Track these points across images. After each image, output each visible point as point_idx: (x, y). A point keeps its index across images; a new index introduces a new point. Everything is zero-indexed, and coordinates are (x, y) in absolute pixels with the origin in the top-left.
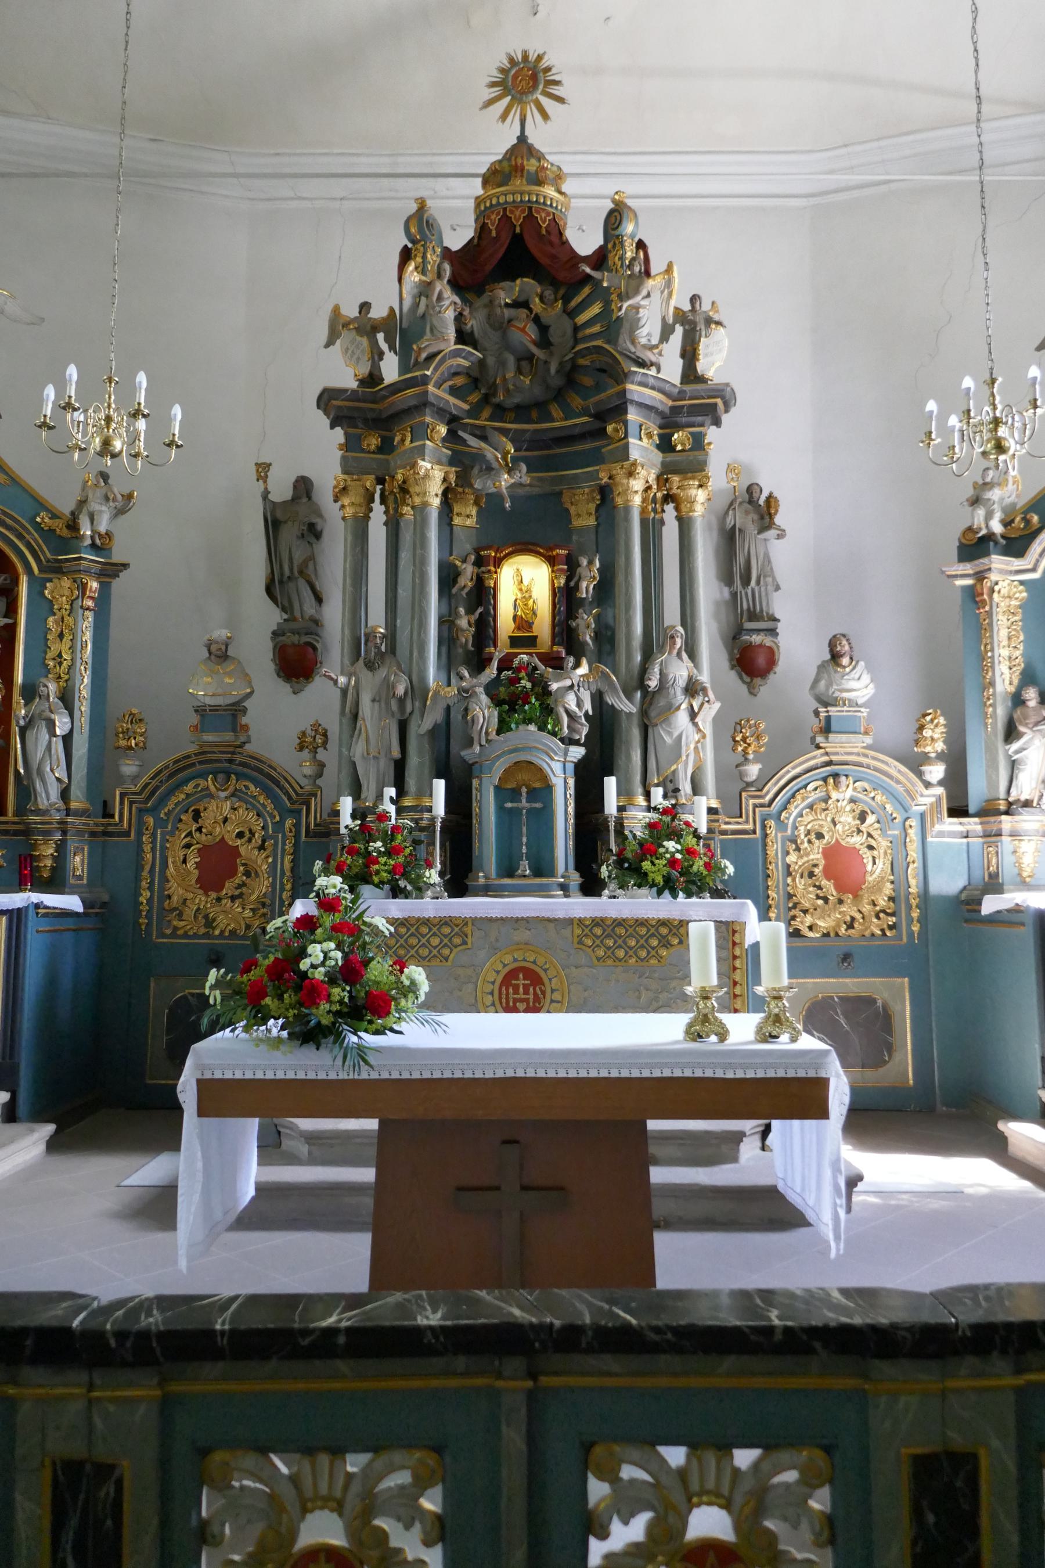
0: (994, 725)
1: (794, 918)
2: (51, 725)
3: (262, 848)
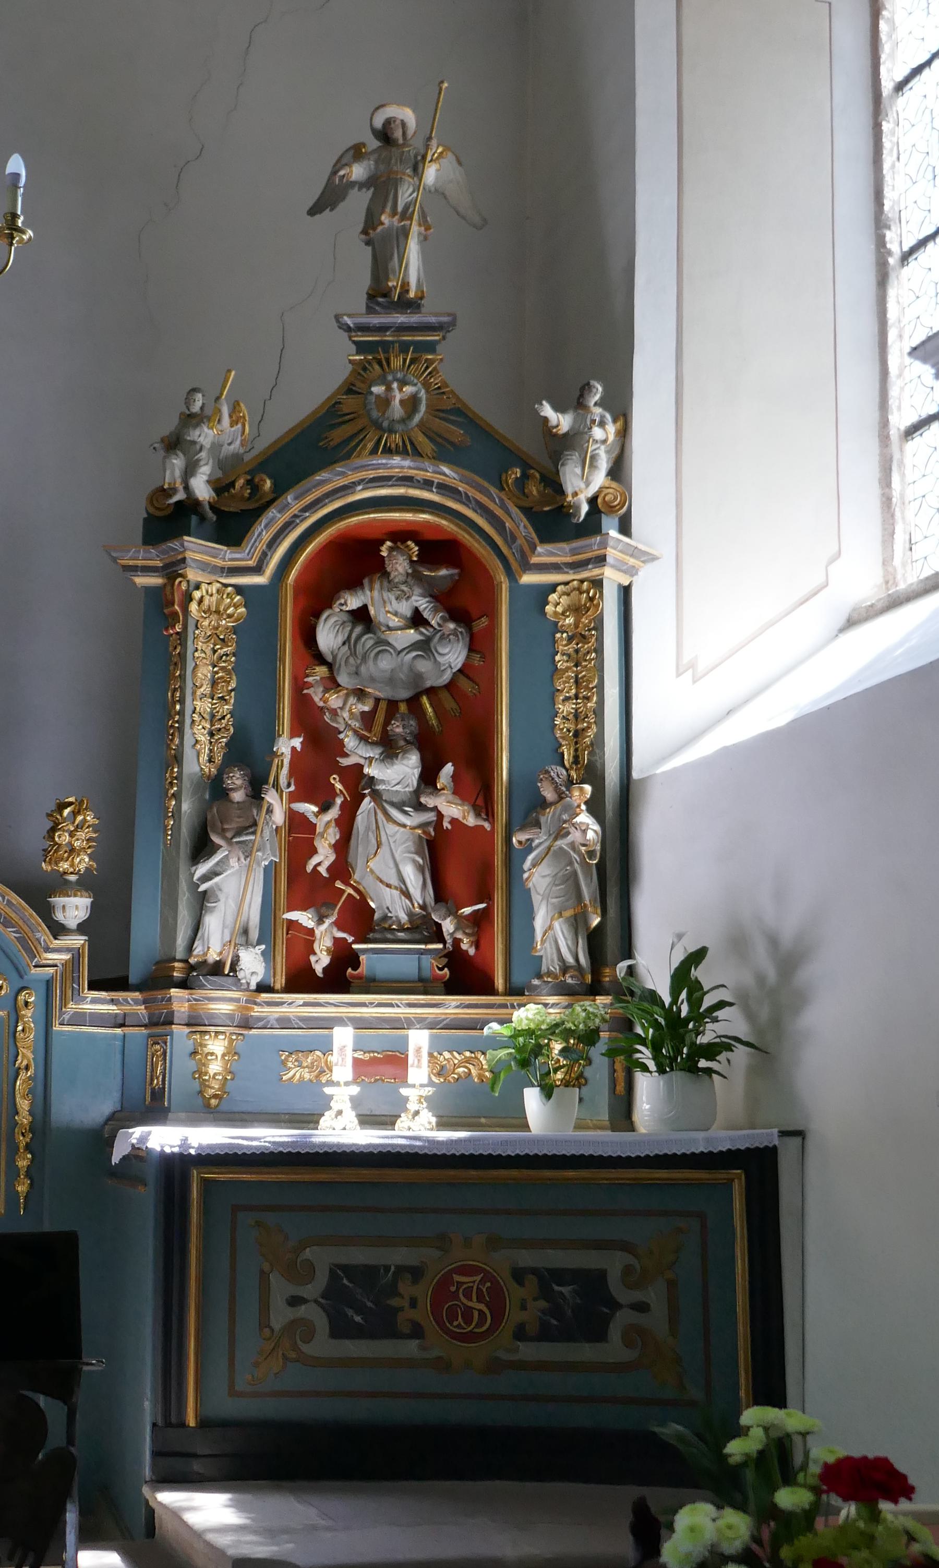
0: (177, 828)
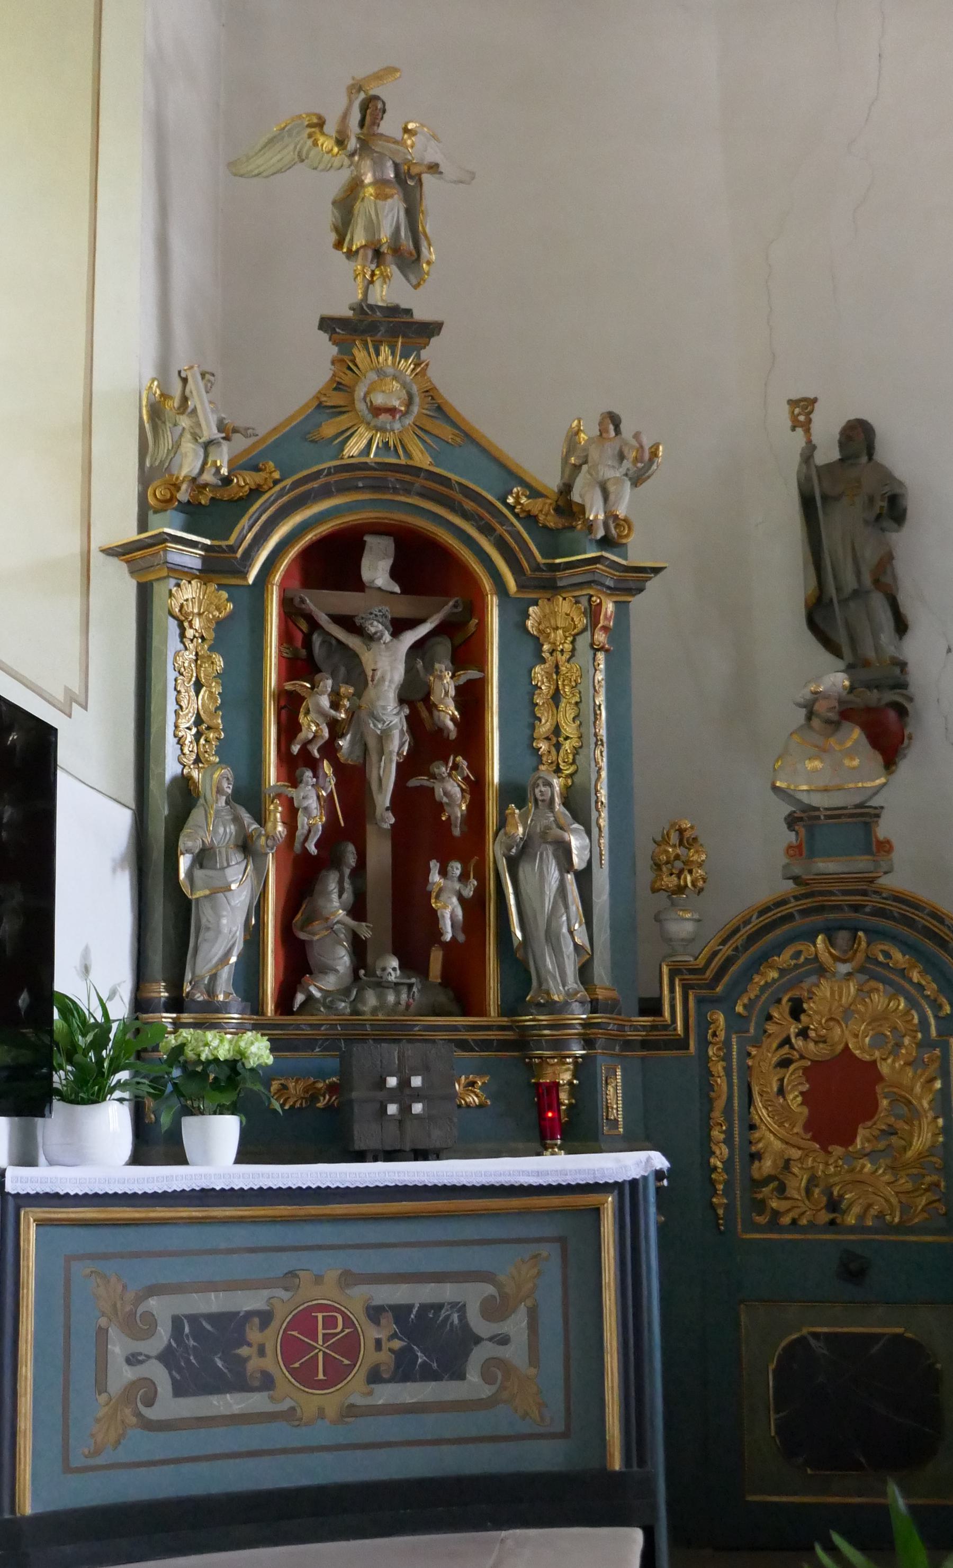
2: (564, 851)
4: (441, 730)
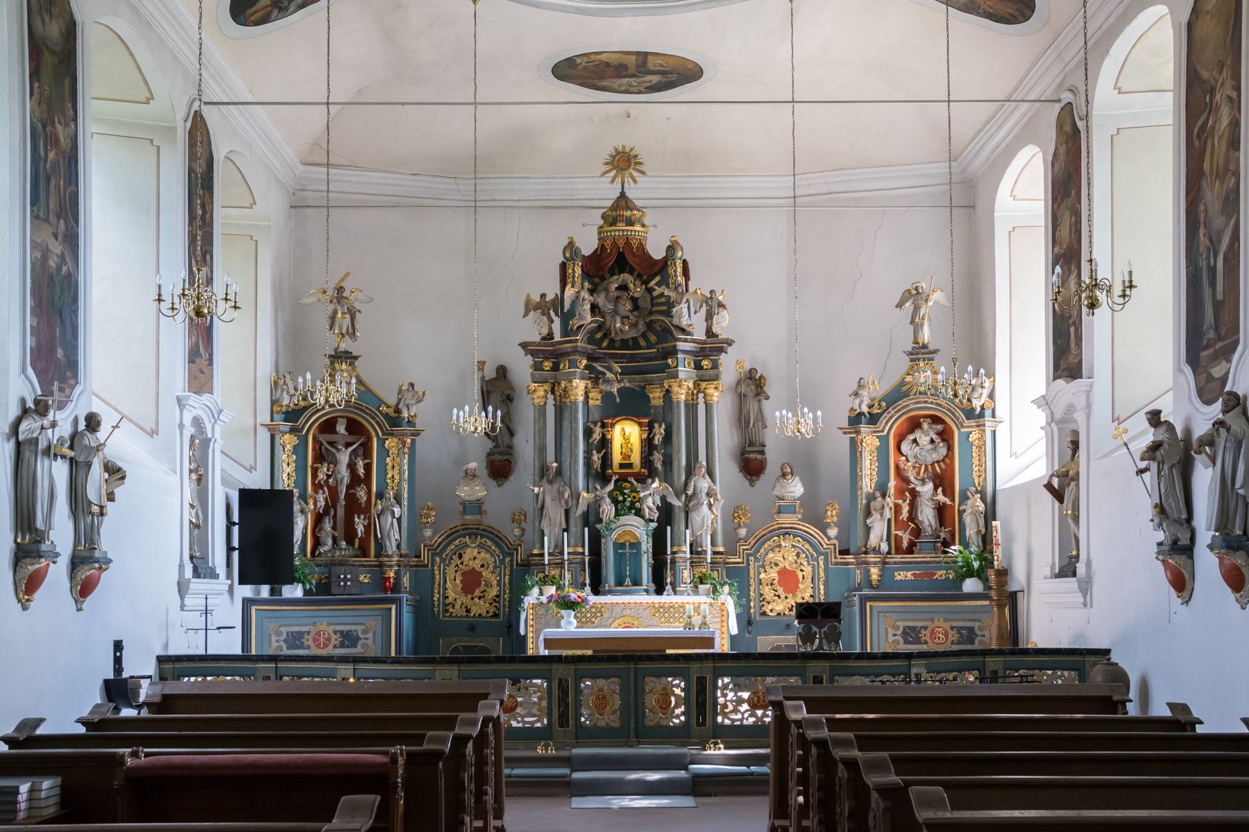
1: (763, 606)
3: (493, 572)
4: (359, 476)
